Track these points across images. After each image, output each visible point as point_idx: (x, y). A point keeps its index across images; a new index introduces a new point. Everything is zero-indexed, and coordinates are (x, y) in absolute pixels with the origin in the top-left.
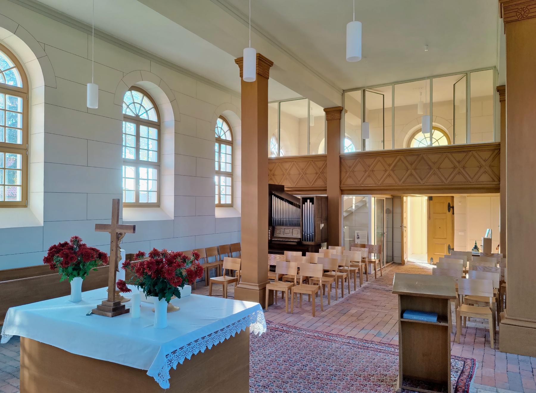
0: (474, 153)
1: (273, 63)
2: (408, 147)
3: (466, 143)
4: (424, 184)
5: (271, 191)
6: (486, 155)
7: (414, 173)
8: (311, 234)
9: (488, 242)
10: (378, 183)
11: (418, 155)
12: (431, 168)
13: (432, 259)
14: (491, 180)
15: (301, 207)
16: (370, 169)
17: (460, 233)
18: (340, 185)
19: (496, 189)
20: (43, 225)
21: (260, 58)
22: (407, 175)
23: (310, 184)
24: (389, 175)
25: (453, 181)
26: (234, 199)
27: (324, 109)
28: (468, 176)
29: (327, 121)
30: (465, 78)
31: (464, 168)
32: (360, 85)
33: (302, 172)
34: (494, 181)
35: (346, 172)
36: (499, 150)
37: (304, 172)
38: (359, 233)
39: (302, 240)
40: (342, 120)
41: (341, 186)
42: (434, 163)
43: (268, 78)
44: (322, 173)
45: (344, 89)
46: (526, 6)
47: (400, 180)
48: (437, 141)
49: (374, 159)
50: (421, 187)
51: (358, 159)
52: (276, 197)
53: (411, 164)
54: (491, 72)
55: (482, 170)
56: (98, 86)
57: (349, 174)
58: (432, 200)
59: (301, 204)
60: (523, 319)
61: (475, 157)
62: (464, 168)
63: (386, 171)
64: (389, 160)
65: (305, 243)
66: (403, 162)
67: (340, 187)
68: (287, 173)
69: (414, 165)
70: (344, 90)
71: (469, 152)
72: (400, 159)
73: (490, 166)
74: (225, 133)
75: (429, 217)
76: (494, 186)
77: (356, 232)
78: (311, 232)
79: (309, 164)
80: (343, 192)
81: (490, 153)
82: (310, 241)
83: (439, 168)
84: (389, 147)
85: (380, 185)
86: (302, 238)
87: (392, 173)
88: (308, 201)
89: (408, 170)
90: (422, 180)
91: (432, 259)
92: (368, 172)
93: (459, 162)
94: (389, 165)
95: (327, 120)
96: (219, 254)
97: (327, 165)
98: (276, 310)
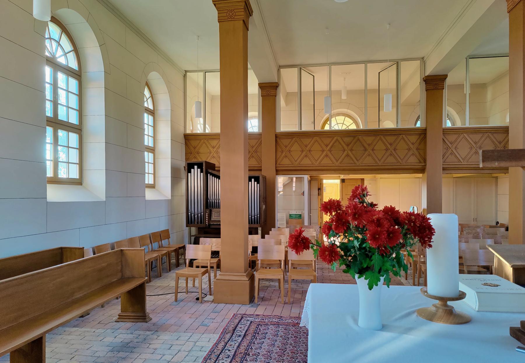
0: (404, 136)
1: (252, 12)
2: (322, 129)
3: (396, 127)
4: (359, 164)
5: (207, 170)
6: (414, 138)
8: (256, 216)
10: (315, 163)
11: (354, 137)
12: (366, 150)
14: (418, 161)
16: (307, 150)
19: (422, 170)
20: (105, 200)
24: (327, 156)
26: (156, 179)
28: (398, 158)
29: (261, 98)
30: (395, 66)
31: (395, 149)
32: (298, 62)
33: (252, 150)
34: (420, 162)
36: (424, 134)
40: (277, 97)
41: (277, 166)
42: (369, 145)
47: (337, 161)
49: (290, 140)
51: (295, 138)
52: (212, 176)
53: (348, 145)
54: (418, 62)
55: (411, 152)
58: (344, 182)
61: (405, 140)
64: (327, 141)
66: (340, 143)
67: (276, 167)
68: (214, 151)
70: (280, 66)
71: (399, 135)
72: (337, 140)
76: (421, 167)
78: (256, 214)
80: (278, 172)
81: (417, 137)
82: (255, 223)
83: (373, 150)
84: (307, 127)
87: (329, 153)
89: (344, 150)
90: (357, 160)
92: (305, 152)
93: (391, 144)
94: (327, 146)
95: (262, 96)
97: (262, 142)
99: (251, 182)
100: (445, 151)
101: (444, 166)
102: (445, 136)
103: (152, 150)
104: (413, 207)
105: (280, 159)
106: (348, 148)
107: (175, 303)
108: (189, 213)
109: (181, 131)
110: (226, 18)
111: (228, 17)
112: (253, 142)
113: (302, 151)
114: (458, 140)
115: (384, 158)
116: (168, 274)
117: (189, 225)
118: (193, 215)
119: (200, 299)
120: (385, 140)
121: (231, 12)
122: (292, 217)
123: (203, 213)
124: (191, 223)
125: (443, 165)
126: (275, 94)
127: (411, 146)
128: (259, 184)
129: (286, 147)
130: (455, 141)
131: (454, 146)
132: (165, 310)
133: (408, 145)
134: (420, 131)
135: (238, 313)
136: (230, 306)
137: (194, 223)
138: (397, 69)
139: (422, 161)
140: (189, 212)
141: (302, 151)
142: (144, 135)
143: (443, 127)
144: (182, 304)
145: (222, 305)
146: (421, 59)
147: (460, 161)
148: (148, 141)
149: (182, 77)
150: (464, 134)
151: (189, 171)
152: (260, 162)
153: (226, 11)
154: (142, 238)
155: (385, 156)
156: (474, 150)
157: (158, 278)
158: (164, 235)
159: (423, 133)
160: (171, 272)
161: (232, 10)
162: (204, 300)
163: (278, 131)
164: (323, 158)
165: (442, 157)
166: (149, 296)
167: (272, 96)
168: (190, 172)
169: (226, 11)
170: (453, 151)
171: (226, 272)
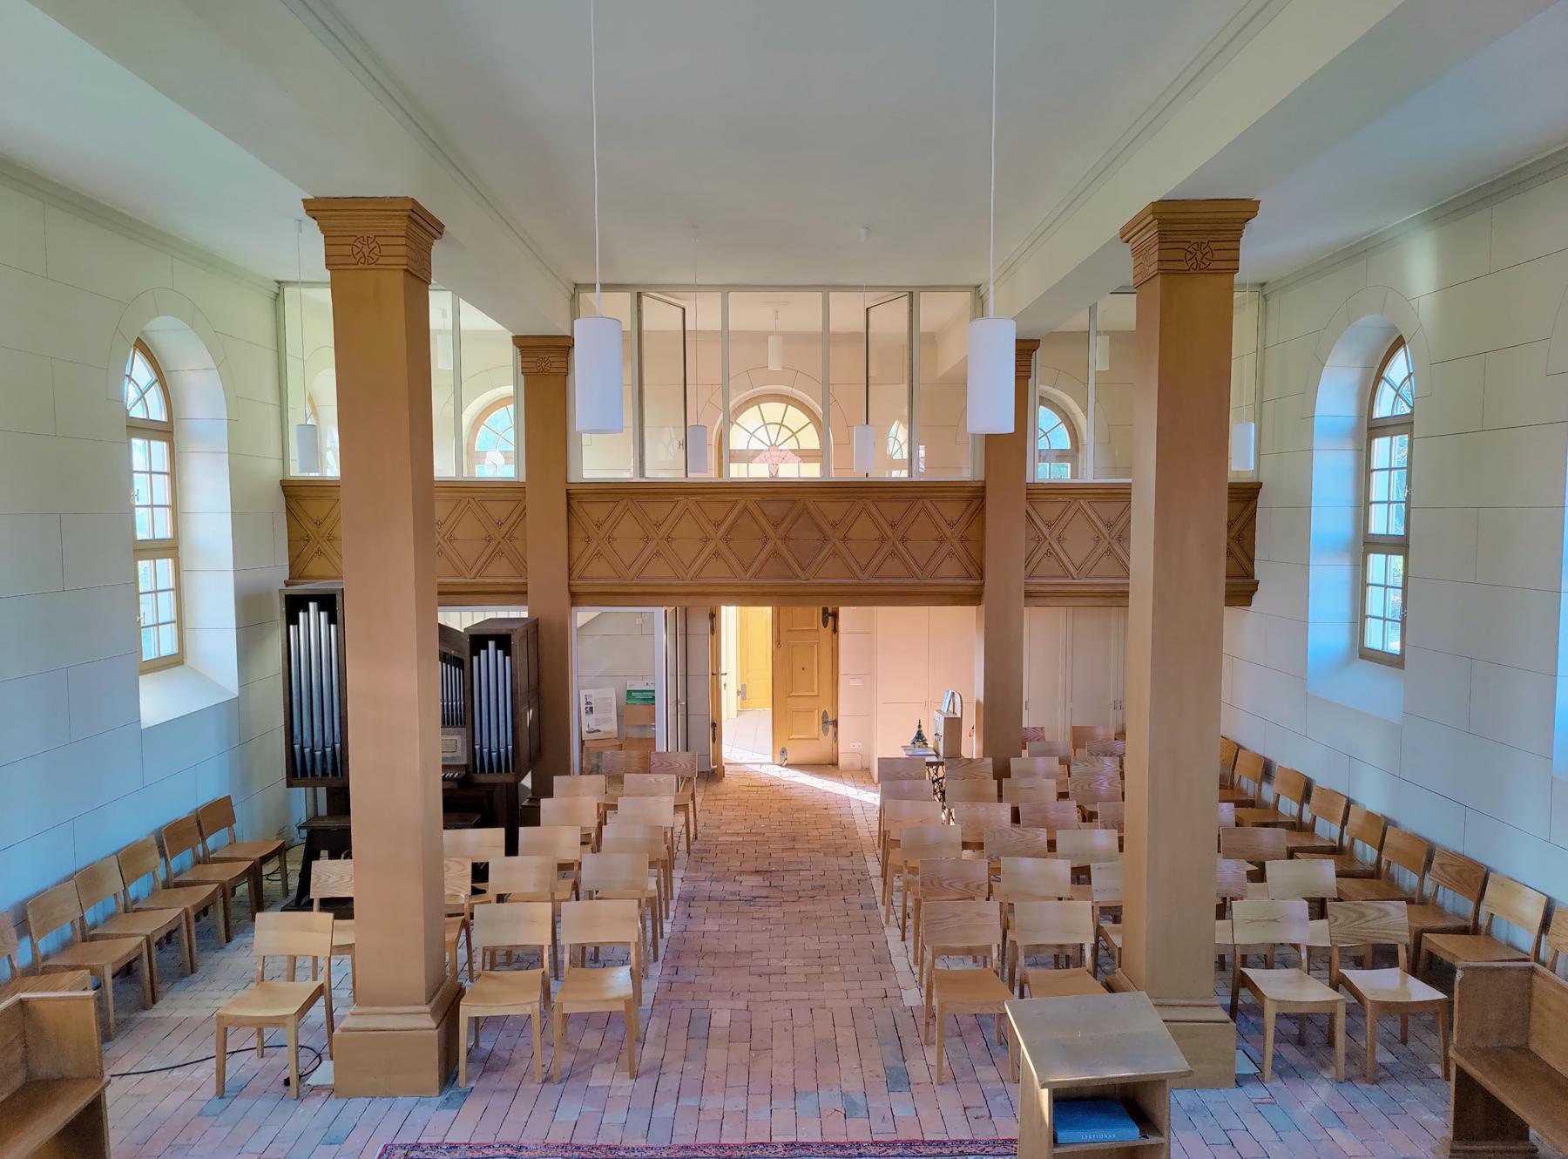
1: (443, 226)
6: (953, 510)
7: (782, 548)
8: (502, 750)
9: (953, 726)
12: (825, 539)
13: (784, 751)
14: (964, 573)
15: (467, 666)
16: (655, 542)
17: (853, 683)
18: (570, 575)
19: (973, 597)
21: (415, 216)
22: (764, 554)
23: (466, 572)
24: (716, 554)
25: (878, 574)
26: (188, 634)
27: (513, 337)
29: (522, 377)
34: (970, 577)
35: (588, 539)
36: (980, 500)
37: (444, 535)
38: (591, 696)
39: (471, 769)
40: (570, 376)
42: (834, 525)
43: (427, 282)
44: (509, 537)
45: (579, 282)
46: (1206, 241)
48: (794, 434)
50: (800, 589)
53: (776, 525)
55: (946, 548)
56: (177, 652)
57: (599, 545)
59: (466, 658)
60: (1177, 1002)
61: (929, 515)
62: (903, 539)
63: (706, 540)
65: (482, 778)
67: (569, 585)
69: (782, 527)
70: (576, 285)
73: (963, 540)
74: (142, 397)
75: (778, 641)
76: (969, 589)
77: (583, 693)
78: (502, 744)
79: (461, 507)
80: (576, 598)
82: (499, 770)
83: (845, 539)
85: (692, 580)
86: (471, 763)
87: (723, 547)
88: (491, 644)
89: (766, 540)
91: (784, 751)
92: (655, 542)
93: (893, 526)
94: (717, 525)
96: (163, 854)
98: (496, 1077)
99: (485, 651)
100: (1033, 544)
101: (1031, 588)
102: (1034, 504)
103: (169, 548)
104: (953, 694)
105: (584, 560)
106: (775, 533)
107: (218, 1105)
108: (297, 747)
109: (271, 471)
110: (352, 260)
111: (358, 257)
112: (501, 510)
113: (647, 539)
114: (1067, 518)
115: (875, 563)
116: (221, 954)
117: (295, 781)
118: (307, 750)
119: (293, 1081)
120: (876, 513)
121: (366, 243)
122: (634, 698)
123: (341, 743)
124: (304, 774)
125: (1026, 584)
126: (565, 370)
127: (948, 531)
128: (510, 655)
129: (599, 525)
130: (1059, 518)
131: (1056, 533)
132: (181, 1140)
133: (937, 526)
134: (969, 492)
135: (397, 1142)
136: (380, 1106)
137: (313, 774)
138: (911, 305)
139: (975, 574)
140: (295, 741)
141: (647, 539)
142: (132, 509)
143: (1028, 481)
144: (239, 1104)
145: (358, 1104)
146: (973, 290)
147: (1069, 575)
148: (150, 524)
149: (267, 304)
150: (1082, 501)
151: (292, 619)
152: (521, 567)
153: (351, 241)
154: (129, 860)
155: (878, 558)
156: (1103, 546)
157: (185, 979)
158: (217, 815)
159: (975, 497)
160: (233, 942)
161: (368, 237)
162: (307, 1082)
163: (572, 479)
164: (707, 561)
165: (1024, 566)
166: (141, 1076)
167: (556, 374)
168: (296, 622)
169: (351, 241)
170: (1053, 548)
171: (373, 1005)
